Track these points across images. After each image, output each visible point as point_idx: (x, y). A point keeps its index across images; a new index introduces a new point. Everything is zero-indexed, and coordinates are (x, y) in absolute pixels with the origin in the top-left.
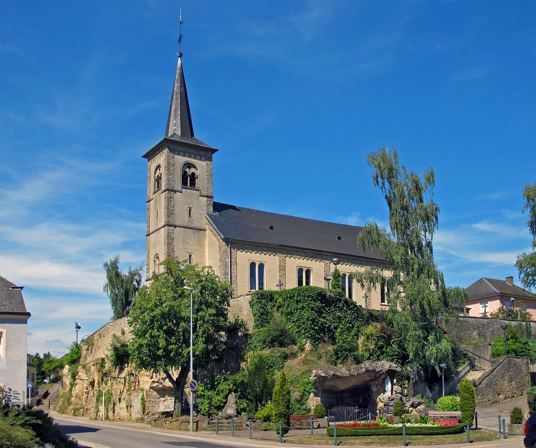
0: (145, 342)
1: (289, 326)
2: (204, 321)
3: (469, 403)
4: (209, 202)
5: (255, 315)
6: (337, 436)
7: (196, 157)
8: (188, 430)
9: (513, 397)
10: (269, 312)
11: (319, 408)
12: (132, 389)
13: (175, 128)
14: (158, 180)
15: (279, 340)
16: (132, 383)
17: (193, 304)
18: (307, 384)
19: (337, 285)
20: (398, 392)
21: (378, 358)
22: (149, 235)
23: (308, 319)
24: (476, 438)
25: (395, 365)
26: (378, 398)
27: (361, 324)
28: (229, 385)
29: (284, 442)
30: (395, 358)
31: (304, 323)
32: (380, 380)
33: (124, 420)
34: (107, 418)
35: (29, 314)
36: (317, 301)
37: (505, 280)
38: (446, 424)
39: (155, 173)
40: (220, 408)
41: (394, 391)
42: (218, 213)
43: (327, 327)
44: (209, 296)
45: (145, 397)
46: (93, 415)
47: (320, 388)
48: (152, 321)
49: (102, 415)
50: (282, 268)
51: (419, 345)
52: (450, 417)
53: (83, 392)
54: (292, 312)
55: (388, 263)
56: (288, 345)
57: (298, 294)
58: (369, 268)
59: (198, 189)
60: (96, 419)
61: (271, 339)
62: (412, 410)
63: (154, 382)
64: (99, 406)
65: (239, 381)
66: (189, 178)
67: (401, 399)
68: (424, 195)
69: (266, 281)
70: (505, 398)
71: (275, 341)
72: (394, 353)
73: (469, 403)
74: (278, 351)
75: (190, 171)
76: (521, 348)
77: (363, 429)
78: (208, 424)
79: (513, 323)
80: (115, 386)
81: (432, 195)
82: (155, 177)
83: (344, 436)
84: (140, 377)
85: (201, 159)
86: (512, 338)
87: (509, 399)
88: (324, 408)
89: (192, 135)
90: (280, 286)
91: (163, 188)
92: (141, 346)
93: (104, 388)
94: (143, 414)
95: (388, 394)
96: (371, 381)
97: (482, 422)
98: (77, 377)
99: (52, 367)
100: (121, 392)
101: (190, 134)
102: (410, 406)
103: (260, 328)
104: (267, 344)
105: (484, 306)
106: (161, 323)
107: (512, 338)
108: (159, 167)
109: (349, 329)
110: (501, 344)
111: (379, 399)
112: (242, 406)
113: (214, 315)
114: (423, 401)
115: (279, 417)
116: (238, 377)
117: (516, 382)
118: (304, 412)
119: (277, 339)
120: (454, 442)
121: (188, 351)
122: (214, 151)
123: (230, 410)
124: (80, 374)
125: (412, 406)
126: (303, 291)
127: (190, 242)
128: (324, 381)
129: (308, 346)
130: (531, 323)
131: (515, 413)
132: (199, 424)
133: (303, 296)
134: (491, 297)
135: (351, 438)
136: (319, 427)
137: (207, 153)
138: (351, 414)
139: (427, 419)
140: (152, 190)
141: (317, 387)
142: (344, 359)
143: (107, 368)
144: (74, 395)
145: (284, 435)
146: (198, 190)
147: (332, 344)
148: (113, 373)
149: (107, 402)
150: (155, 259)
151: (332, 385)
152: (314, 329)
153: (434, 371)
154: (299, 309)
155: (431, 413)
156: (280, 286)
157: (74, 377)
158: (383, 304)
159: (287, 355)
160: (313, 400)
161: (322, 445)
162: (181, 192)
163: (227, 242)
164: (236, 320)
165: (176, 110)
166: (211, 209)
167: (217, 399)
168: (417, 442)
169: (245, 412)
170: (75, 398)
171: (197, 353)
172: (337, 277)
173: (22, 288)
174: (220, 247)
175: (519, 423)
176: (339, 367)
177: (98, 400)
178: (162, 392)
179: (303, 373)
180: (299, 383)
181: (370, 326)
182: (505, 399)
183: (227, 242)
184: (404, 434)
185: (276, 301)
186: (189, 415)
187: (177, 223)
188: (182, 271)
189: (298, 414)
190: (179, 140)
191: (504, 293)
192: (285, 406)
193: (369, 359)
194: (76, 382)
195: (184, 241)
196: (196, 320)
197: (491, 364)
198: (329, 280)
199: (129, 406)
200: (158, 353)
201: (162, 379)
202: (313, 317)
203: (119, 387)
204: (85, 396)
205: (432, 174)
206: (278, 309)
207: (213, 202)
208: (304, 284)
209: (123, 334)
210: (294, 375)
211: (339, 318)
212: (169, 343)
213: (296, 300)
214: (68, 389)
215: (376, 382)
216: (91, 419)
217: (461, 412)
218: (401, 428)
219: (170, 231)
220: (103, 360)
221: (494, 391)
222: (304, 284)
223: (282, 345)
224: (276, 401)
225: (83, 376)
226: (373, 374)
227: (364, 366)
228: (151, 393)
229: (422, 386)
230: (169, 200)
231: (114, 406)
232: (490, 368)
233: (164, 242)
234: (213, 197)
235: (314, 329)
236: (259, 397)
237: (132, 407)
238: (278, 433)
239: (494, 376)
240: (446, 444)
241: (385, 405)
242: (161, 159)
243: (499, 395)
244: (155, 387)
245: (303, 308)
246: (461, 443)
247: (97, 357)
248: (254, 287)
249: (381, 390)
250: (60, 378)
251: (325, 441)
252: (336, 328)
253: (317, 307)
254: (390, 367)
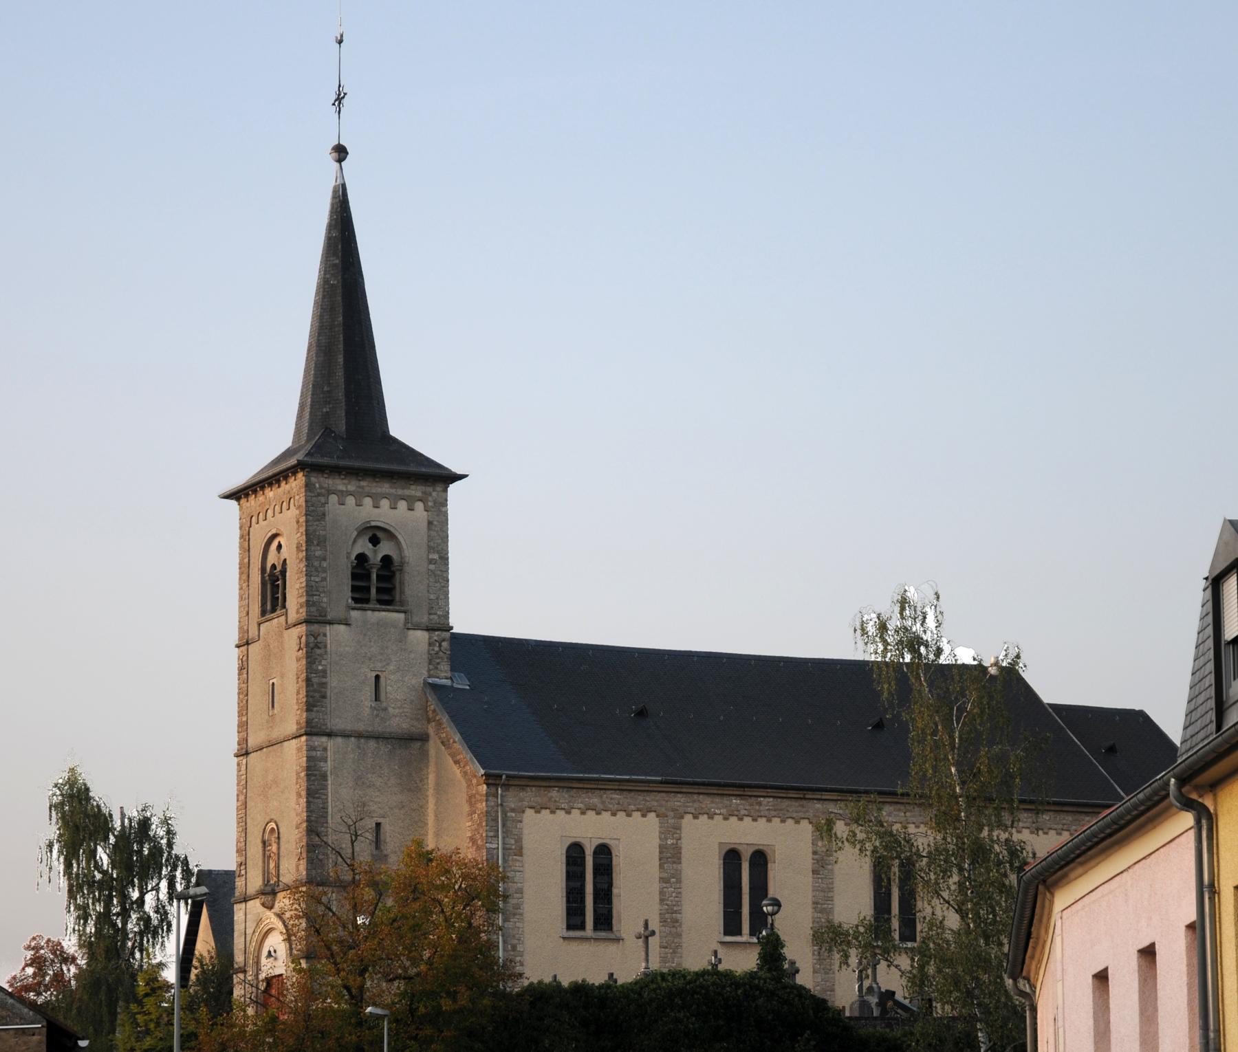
7: (396, 503)
50: (670, 855)
51: (431, 919)
82: (263, 569)
187: (336, 723)
219: (314, 754)
230: (313, 650)
233: (294, 788)
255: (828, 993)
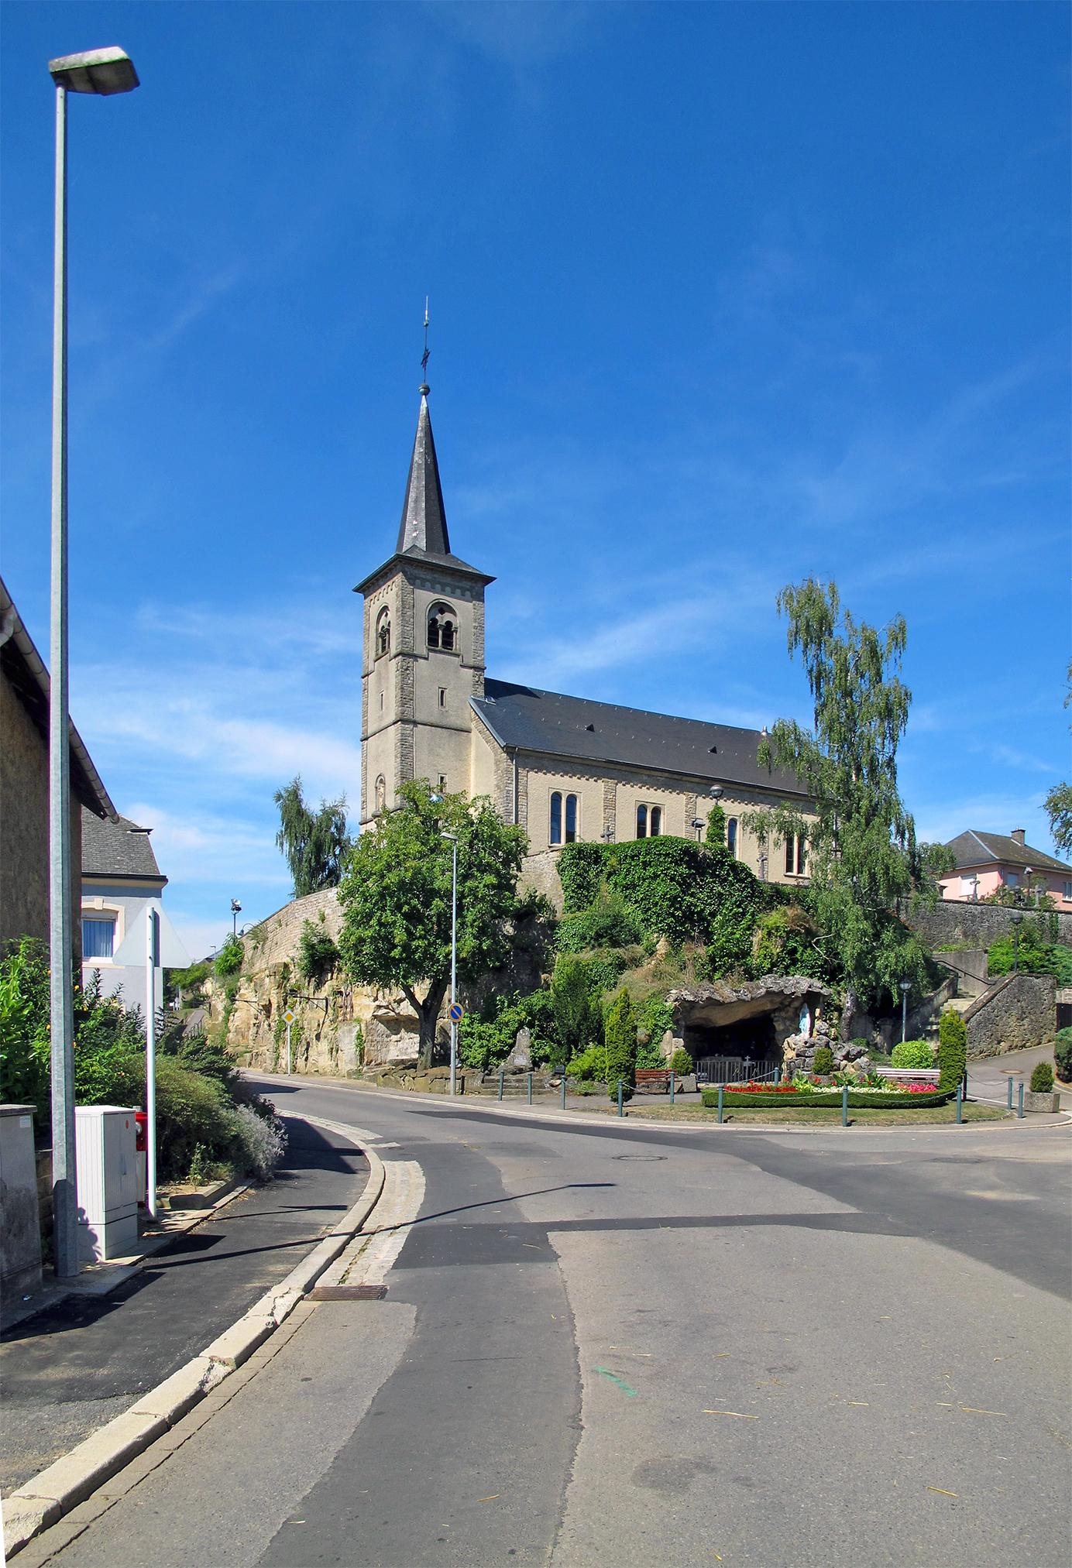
0: (369, 933)
1: (628, 909)
2: (476, 897)
3: (956, 1055)
4: (477, 679)
5: (565, 890)
6: (724, 1107)
8: (445, 1092)
9: (1024, 1046)
10: (592, 882)
11: (682, 1057)
12: (340, 1018)
13: (415, 534)
14: (384, 635)
15: (610, 934)
16: (340, 1009)
17: (457, 865)
18: (661, 1014)
19: (717, 835)
20: (823, 1032)
21: (786, 971)
22: (366, 739)
23: (663, 897)
24: (970, 1117)
25: (819, 984)
26: (786, 1042)
27: (758, 908)
28: (518, 1014)
29: (627, 1115)
30: (817, 972)
31: (656, 904)
32: (791, 1010)
33: (324, 1074)
34: (294, 1069)
35: (164, 879)
36: (681, 865)
37: (1010, 835)
38: (916, 1090)
39: (378, 622)
40: (502, 1055)
41: (814, 1030)
42: (493, 700)
43: (697, 913)
44: (485, 851)
45: (364, 1033)
46: (270, 1067)
47: (684, 1023)
48: (382, 896)
49: (286, 1065)
50: (610, 805)
52: (915, 1079)
53: (248, 1024)
54: (634, 884)
55: (806, 802)
56: (627, 942)
57: (646, 850)
58: (766, 808)
59: (458, 652)
60: (274, 1071)
61: (596, 932)
62: (846, 1065)
63: (379, 1007)
64: (281, 1048)
65: (538, 1008)
66: (440, 632)
67: (827, 1045)
68: (884, 667)
69: (580, 828)
70: (1010, 1048)
71: (602, 937)
72: (816, 963)
73: (956, 1055)
74: (608, 954)
75: (443, 619)
76: (1040, 960)
77: (768, 1095)
78: (483, 1082)
79: (1028, 915)
80: (309, 1014)
81: (898, 667)
82: (377, 630)
83: (733, 1107)
84: (353, 998)
85: (462, 597)
86: (1024, 940)
87: (1016, 1051)
88: (690, 1058)
89: (448, 550)
90: (608, 836)
91: (393, 650)
92: (361, 941)
93: (289, 1017)
94: (361, 1063)
95: (805, 1035)
96: (775, 1010)
97: (974, 1089)
98: (237, 997)
99: (189, 980)
100: (319, 1025)
101: (443, 548)
102: (842, 1059)
103: (575, 912)
104: (587, 941)
105: (974, 882)
106: (399, 899)
107: (1024, 940)
108: (385, 608)
109: (738, 917)
110: (1005, 951)
111: (788, 1044)
112: (541, 1052)
113: (494, 887)
114: (867, 1050)
115: (617, 1071)
116: (537, 999)
117: (1032, 1020)
118: (653, 1064)
119: (606, 932)
120: (932, 1121)
121: (447, 951)
122: (489, 580)
123: (521, 1058)
124: (242, 991)
125: (846, 1057)
126: (656, 846)
127: (443, 753)
128: (691, 1009)
129: (662, 947)
130: (1060, 915)
131: (1040, 1072)
132: (465, 1082)
133: (655, 854)
134: (984, 867)
135: (746, 1111)
136: (681, 1091)
137: (474, 585)
138: (737, 1071)
139: (881, 1081)
140: (373, 656)
141: (678, 1020)
142: (726, 972)
143: (293, 981)
144: (232, 1029)
145: (625, 1104)
146: (457, 655)
147: (705, 944)
148: (305, 990)
149: (294, 1042)
150: (378, 783)
151: (704, 1017)
152: (673, 915)
153: (888, 996)
154: (648, 879)
155: (881, 1070)
156: (608, 836)
157: (232, 997)
158: (800, 875)
159: (624, 961)
160: (670, 1043)
161: (696, 1121)
162: (427, 659)
163: (511, 753)
164: (530, 896)
165: (416, 501)
166: (481, 691)
167: (498, 1039)
168: (866, 1120)
169: (547, 1062)
170: (235, 1034)
171: (463, 955)
172: (717, 821)
173: (148, 831)
174: (497, 762)
175: (1046, 1091)
176: (719, 985)
177: (278, 1038)
178: (395, 1024)
179: (653, 994)
180: (645, 1012)
181: (774, 913)
182: (1009, 1050)
183: (511, 753)
184: (845, 1105)
185: (605, 863)
186: (448, 1063)
187: (418, 717)
188: (434, 804)
189: (643, 1068)
190: (422, 558)
191: (1007, 859)
192: (627, 1052)
193: (770, 971)
194: (235, 1006)
195: (431, 752)
196: (462, 896)
197: (986, 987)
198: (700, 826)
199: (334, 1050)
200: (392, 954)
201: (395, 1001)
202: (673, 892)
203: (315, 1015)
204: (253, 1030)
205: (902, 630)
206: (608, 878)
207: (485, 678)
208: (648, 834)
209: (323, 921)
210: (638, 999)
211: (720, 894)
212: (411, 935)
213: (643, 862)
214: (220, 1018)
215: (783, 1014)
216: (265, 1071)
217: (939, 1071)
218: (839, 1095)
219: (405, 732)
220: (286, 966)
221: (992, 1035)
222: (648, 834)
223: (615, 943)
224: (611, 1042)
225: (248, 995)
226: (778, 999)
227: (762, 985)
228: (374, 1027)
229: (863, 1023)
230: (405, 672)
231: (307, 1049)
232: (986, 993)
234: (486, 668)
235: (673, 915)
236: (573, 1035)
237: (339, 1051)
238: (615, 1100)
239: (994, 1009)
240: (917, 1124)
241: (798, 1055)
242: (390, 594)
243: (999, 1043)
244: (380, 1016)
245: (655, 876)
246: (945, 1123)
247: (274, 962)
248: (557, 838)
249: (790, 1028)
250: (202, 999)
251: (700, 1115)
252: (713, 915)
253: (680, 875)
254: (810, 987)
255: (461, 857)
